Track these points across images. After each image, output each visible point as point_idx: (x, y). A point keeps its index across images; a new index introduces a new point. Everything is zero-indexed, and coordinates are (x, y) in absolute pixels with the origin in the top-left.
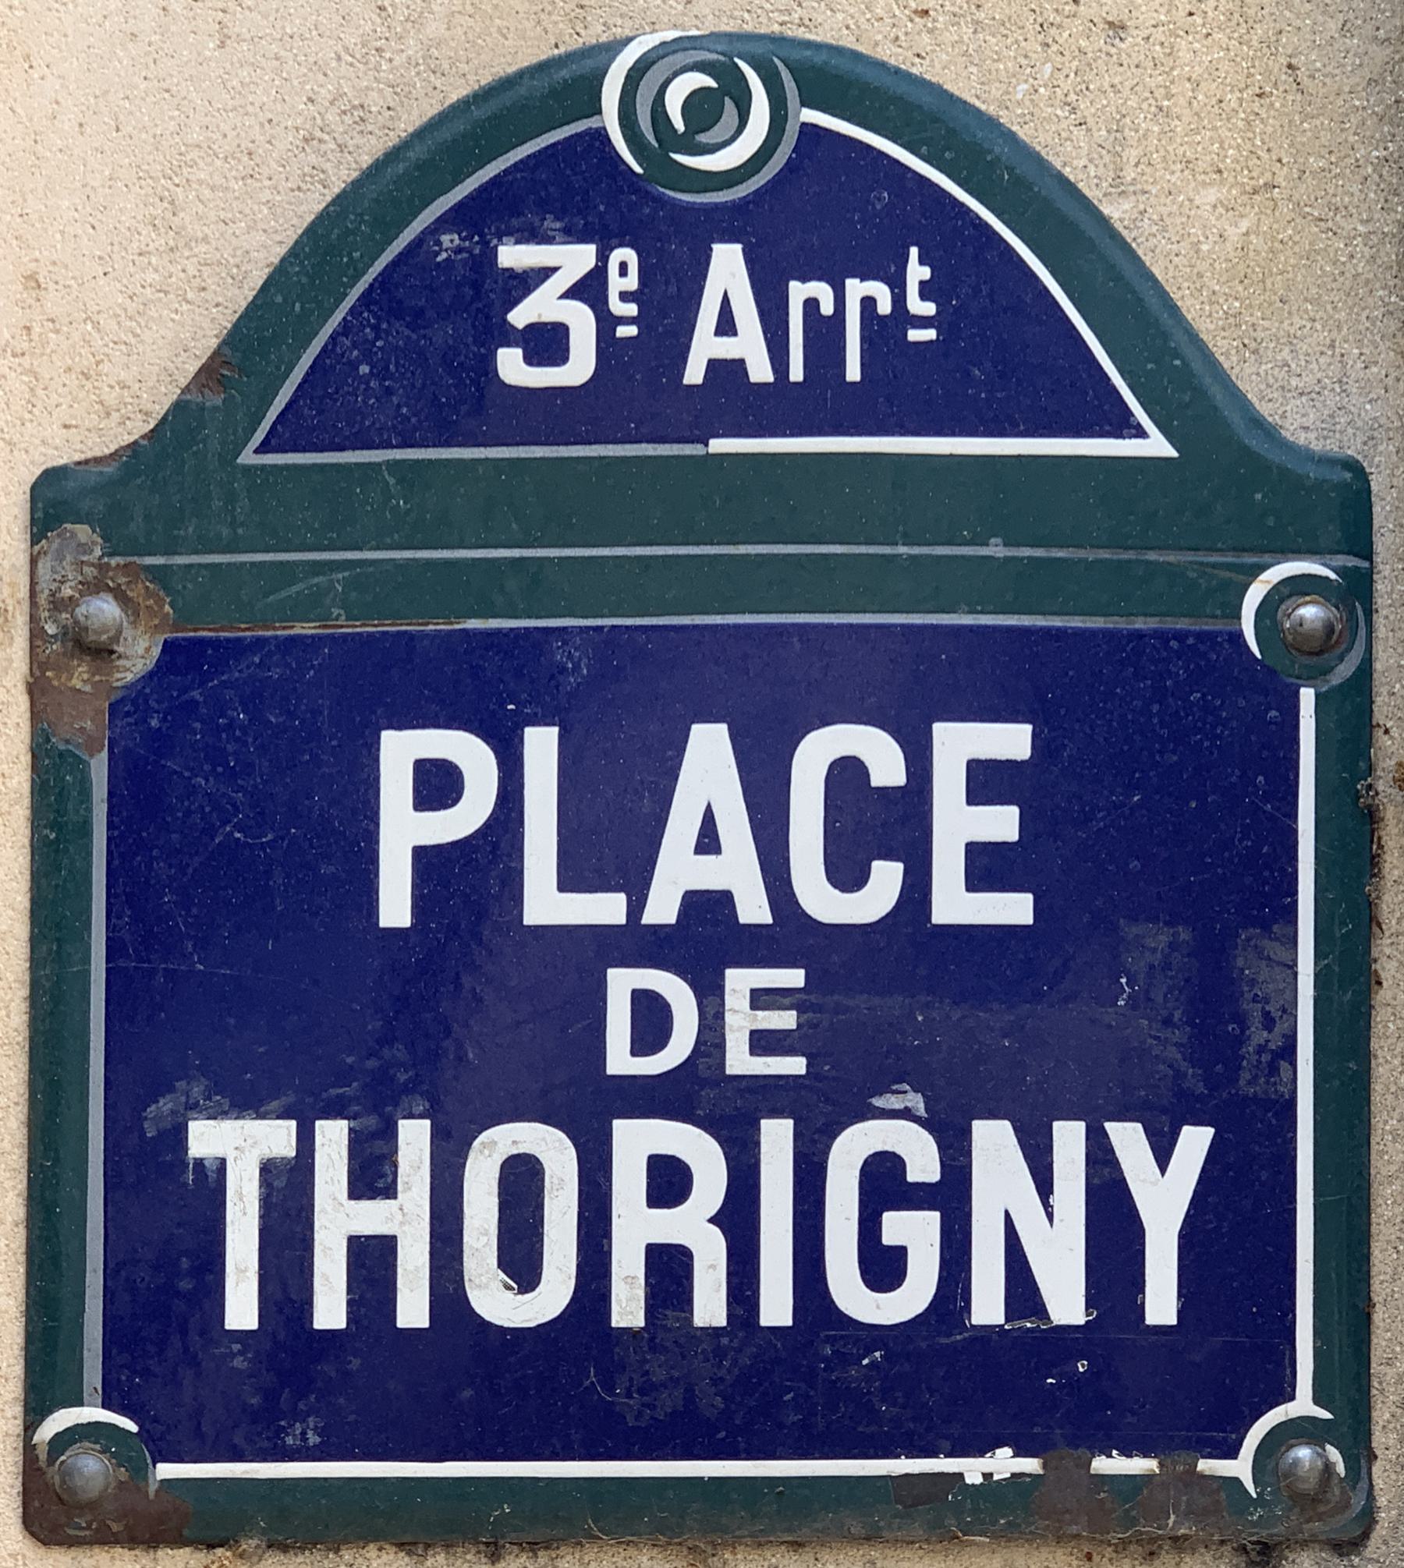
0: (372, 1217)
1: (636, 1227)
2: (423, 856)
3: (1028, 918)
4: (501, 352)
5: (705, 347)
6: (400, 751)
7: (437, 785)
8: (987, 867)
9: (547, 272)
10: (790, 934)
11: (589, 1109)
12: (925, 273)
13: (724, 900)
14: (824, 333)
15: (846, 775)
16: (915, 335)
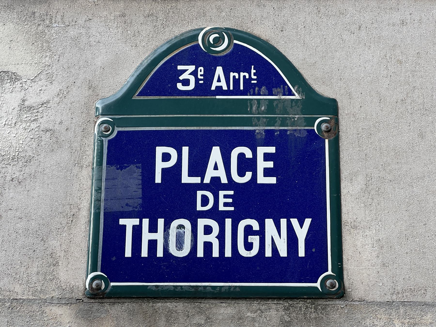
0: (153, 236)
1: (202, 238)
2: (163, 170)
3: (272, 166)
4: (178, 84)
5: (215, 84)
6: (160, 150)
7: (166, 157)
8: (267, 172)
9: (186, 70)
10: (231, 185)
11: (194, 217)
12: (255, 71)
13: (218, 179)
14: (236, 82)
15: (241, 156)
16: (253, 82)
